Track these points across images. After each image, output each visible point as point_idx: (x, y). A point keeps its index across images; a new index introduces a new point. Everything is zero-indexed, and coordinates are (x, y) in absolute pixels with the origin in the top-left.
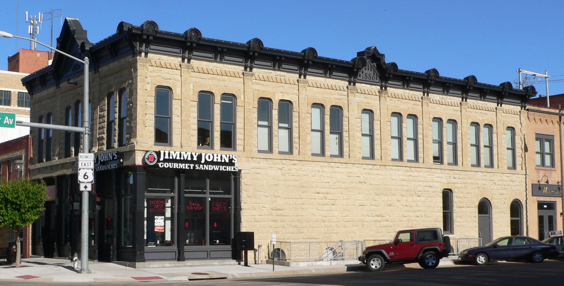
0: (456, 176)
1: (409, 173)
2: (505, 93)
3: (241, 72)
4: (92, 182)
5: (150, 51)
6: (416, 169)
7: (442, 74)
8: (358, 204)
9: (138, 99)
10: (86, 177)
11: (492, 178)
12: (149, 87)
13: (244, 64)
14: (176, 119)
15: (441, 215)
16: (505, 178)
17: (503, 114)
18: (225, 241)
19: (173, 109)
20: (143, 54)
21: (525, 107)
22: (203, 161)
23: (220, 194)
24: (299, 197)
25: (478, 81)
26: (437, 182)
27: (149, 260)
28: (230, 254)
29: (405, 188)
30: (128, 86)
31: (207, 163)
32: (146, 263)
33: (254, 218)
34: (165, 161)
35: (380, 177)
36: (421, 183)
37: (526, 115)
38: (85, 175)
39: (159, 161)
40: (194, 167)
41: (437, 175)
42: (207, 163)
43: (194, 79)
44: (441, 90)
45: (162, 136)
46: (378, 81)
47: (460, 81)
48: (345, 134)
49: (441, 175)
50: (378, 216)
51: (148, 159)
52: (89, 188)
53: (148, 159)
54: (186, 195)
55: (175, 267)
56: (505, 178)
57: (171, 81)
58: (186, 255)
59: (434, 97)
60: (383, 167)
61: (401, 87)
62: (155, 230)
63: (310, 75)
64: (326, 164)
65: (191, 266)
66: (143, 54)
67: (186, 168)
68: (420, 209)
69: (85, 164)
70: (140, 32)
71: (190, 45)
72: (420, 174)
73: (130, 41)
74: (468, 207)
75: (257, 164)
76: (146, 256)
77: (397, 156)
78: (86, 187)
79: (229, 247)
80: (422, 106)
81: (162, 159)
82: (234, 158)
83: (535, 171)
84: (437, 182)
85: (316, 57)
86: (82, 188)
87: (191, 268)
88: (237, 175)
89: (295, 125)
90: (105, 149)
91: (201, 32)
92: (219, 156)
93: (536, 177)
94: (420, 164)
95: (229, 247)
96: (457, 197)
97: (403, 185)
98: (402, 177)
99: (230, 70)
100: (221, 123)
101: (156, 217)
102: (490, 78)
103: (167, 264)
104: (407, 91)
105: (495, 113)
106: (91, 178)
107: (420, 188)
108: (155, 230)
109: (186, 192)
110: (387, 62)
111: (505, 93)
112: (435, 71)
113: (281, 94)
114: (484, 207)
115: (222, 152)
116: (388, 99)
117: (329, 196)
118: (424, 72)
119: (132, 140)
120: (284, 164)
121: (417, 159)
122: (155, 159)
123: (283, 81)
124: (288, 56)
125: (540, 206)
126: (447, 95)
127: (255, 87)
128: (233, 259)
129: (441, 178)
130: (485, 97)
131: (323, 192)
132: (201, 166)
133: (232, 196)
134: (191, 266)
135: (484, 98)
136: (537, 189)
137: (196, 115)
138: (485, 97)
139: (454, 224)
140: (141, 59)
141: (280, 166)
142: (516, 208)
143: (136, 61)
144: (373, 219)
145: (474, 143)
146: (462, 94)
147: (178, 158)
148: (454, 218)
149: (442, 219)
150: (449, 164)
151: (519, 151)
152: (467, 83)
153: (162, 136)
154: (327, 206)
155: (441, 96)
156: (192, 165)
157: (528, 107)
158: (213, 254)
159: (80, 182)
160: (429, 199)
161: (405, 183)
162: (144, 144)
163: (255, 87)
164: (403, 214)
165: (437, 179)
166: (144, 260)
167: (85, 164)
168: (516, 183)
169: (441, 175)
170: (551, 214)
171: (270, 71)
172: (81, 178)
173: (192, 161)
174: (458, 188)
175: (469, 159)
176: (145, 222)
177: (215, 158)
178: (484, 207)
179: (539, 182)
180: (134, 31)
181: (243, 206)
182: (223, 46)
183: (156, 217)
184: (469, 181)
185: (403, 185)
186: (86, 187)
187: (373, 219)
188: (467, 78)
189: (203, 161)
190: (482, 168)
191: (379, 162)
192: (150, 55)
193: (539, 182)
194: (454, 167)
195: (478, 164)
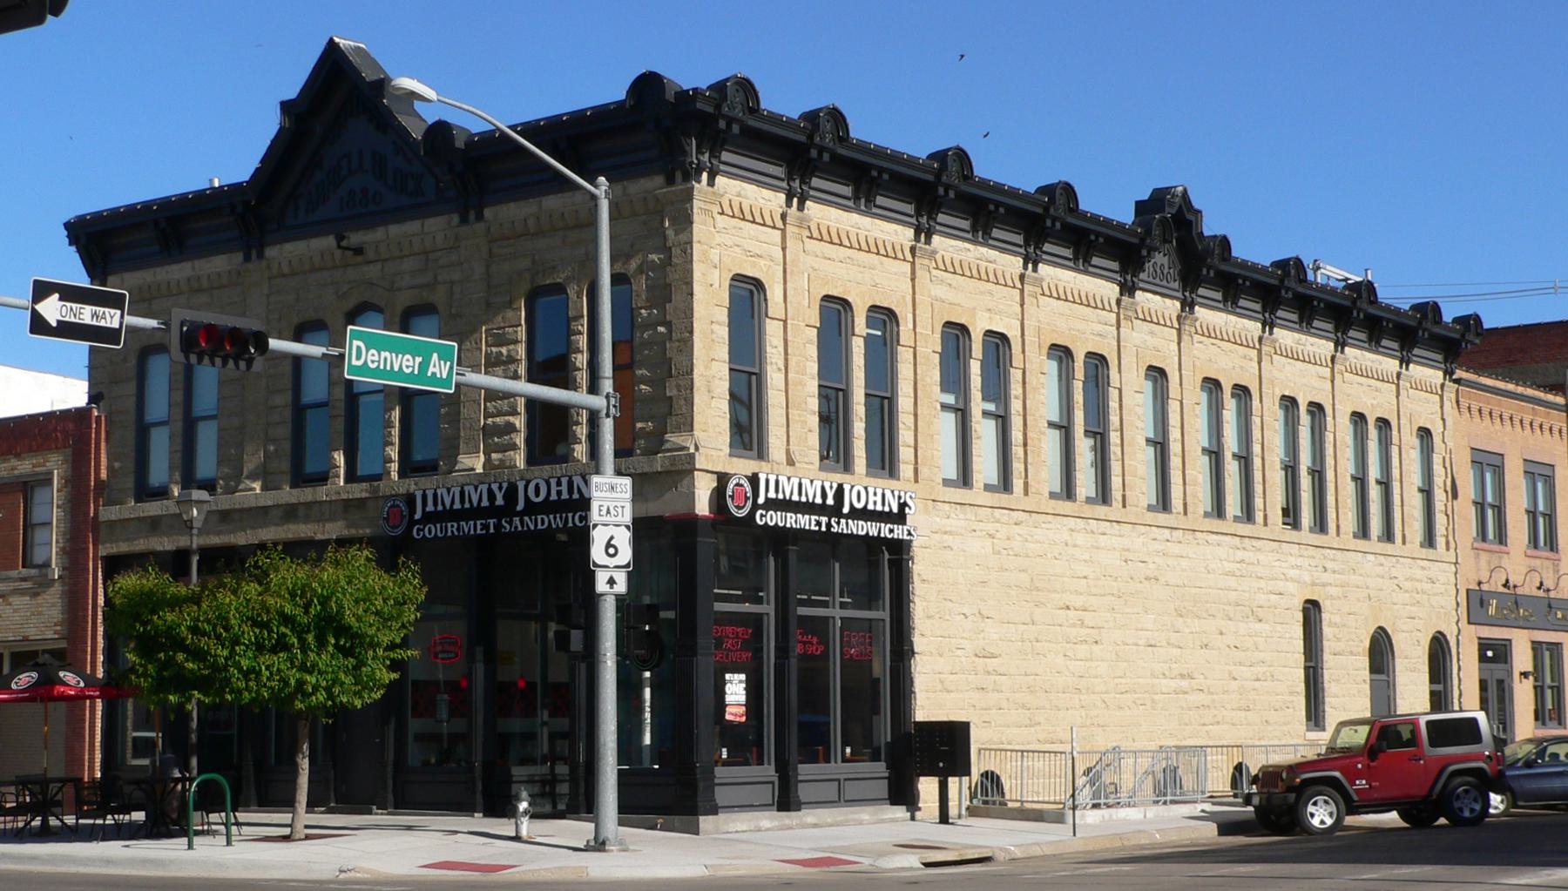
0: (1330, 565)
1: (1240, 555)
2: (1054, 220)
3: (908, 245)
4: (628, 566)
5: (722, 167)
6: (1254, 542)
7: (984, 168)
8: (1142, 642)
9: (696, 314)
10: (611, 551)
11: (1394, 573)
12: (715, 276)
13: (784, 185)
14: (774, 378)
15: (1301, 673)
16: (1419, 574)
17: (935, 272)
18: (865, 748)
19: (769, 349)
20: (705, 176)
21: (1452, 373)
22: (846, 510)
23: (737, 599)
24: (1028, 620)
25: (1082, 206)
26: (1293, 580)
27: (730, 808)
28: (882, 788)
29: (1233, 596)
30: (640, 270)
31: (856, 514)
32: (722, 816)
33: (942, 682)
34: (772, 504)
35: (1184, 563)
36: (1262, 583)
37: (1453, 396)
38: (609, 545)
39: (755, 506)
40: (829, 525)
41: (1292, 560)
42: (856, 514)
43: (810, 260)
44: (966, 224)
45: (748, 431)
46: (1176, 285)
47: (911, 162)
48: (1114, 437)
49: (1299, 561)
50: (1182, 676)
51: (732, 497)
52: (621, 587)
53: (732, 497)
54: (720, 607)
55: (781, 829)
56: (1419, 574)
57: (763, 262)
58: (804, 792)
59: (1355, 355)
60: (1189, 535)
61: (850, 203)
62: (728, 717)
63: (1202, 305)
64: (1081, 523)
65: (815, 826)
66: (705, 176)
67: (813, 528)
68: (1261, 656)
69: (608, 512)
70: (711, 110)
71: (816, 156)
72: (1261, 557)
73: (663, 134)
74: (1352, 653)
75: (945, 521)
76: (721, 795)
77: (952, 472)
78: (611, 582)
79: (880, 768)
80: (1259, 363)
81: (761, 500)
82: (909, 502)
83: (1472, 553)
84: (1293, 580)
85: (755, 110)
86: (601, 586)
87: (815, 830)
88: (899, 551)
89: (1016, 406)
90: (520, 459)
91: (757, 87)
92: (879, 492)
93: (1479, 568)
94: (1115, 510)
95: (880, 768)
96: (1331, 624)
97: (1228, 589)
98: (1229, 566)
99: (886, 238)
100: (820, 386)
101: (728, 676)
102: (893, 125)
103: (865, 814)
104: (1233, 318)
105: (908, 267)
106: (626, 555)
107: (1262, 598)
108: (728, 717)
109: (803, 603)
110: (1207, 232)
111: (1054, 220)
112: (746, 87)
113: (987, 315)
114: (1381, 651)
115: (824, 475)
116: (1196, 337)
117: (1088, 618)
118: (795, 115)
119: (673, 438)
120: (998, 521)
121: (1164, 503)
122: (747, 499)
123: (992, 278)
124: (1255, 276)
125: (1484, 645)
126: (1309, 333)
127: (939, 291)
128: (893, 803)
129: (1285, 566)
130: (987, 233)
131: (1078, 605)
132: (843, 521)
133: (883, 614)
134: (815, 826)
135: (868, 201)
136: (1477, 603)
137: (813, 367)
138: (870, 201)
139: (1327, 700)
140: (701, 186)
141: (991, 527)
142: (1439, 651)
143: (689, 196)
144: (1174, 684)
145: (1055, 418)
146: (918, 214)
147: (795, 498)
148: (1326, 685)
149: (1303, 685)
150: (988, 488)
151: (1440, 496)
152: (1354, 301)
153: (748, 431)
154: (1084, 646)
155: (1296, 335)
156: (824, 520)
157: (1459, 374)
158: (851, 790)
159: (596, 565)
160: (1279, 628)
161: (1232, 582)
162: (713, 452)
163: (939, 291)
164: (1230, 673)
165: (1293, 573)
166: (714, 810)
167: (608, 512)
168: (1438, 587)
169: (1299, 561)
170: (1501, 675)
171: (967, 245)
172: (597, 553)
173: (821, 509)
174: (1332, 597)
175: (1044, 475)
176: (647, 692)
177: (872, 498)
178: (1381, 651)
179: (1480, 583)
180: (699, 105)
181: (919, 642)
182: (886, 165)
183: (728, 676)
184: (1353, 578)
185: (1228, 589)
186: (611, 582)
187: (1174, 684)
188: (811, 117)
189: (846, 510)
190: (977, 494)
191: (1181, 521)
192: (720, 180)
193: (1480, 583)
194: (1003, 499)
195: (965, 477)
